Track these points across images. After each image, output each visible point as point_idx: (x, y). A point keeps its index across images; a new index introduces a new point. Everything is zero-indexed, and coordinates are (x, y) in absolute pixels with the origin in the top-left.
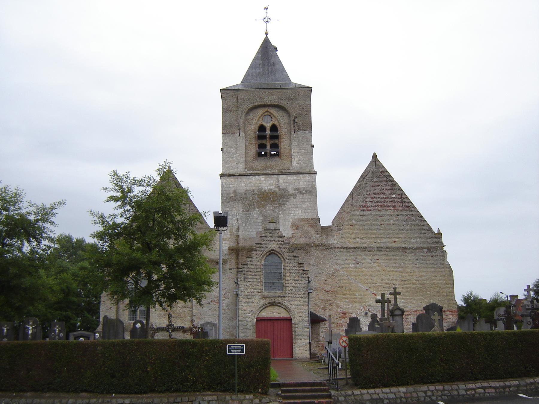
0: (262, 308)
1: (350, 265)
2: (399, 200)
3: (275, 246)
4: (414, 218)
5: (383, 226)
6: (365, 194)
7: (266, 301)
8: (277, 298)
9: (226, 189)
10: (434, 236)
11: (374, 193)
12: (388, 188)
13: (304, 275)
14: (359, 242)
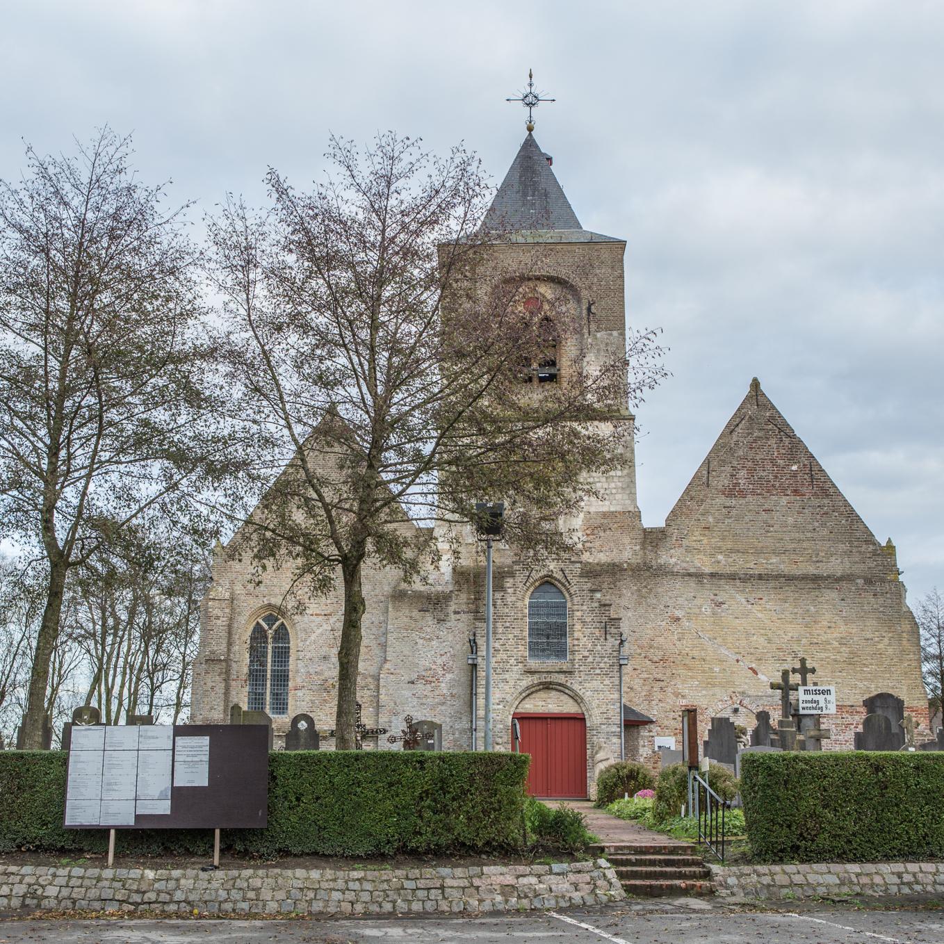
0: (524, 695)
2: (806, 476)
5: (772, 529)
6: (735, 463)
7: (535, 679)
11: (753, 460)
12: (784, 452)
14: (724, 563)
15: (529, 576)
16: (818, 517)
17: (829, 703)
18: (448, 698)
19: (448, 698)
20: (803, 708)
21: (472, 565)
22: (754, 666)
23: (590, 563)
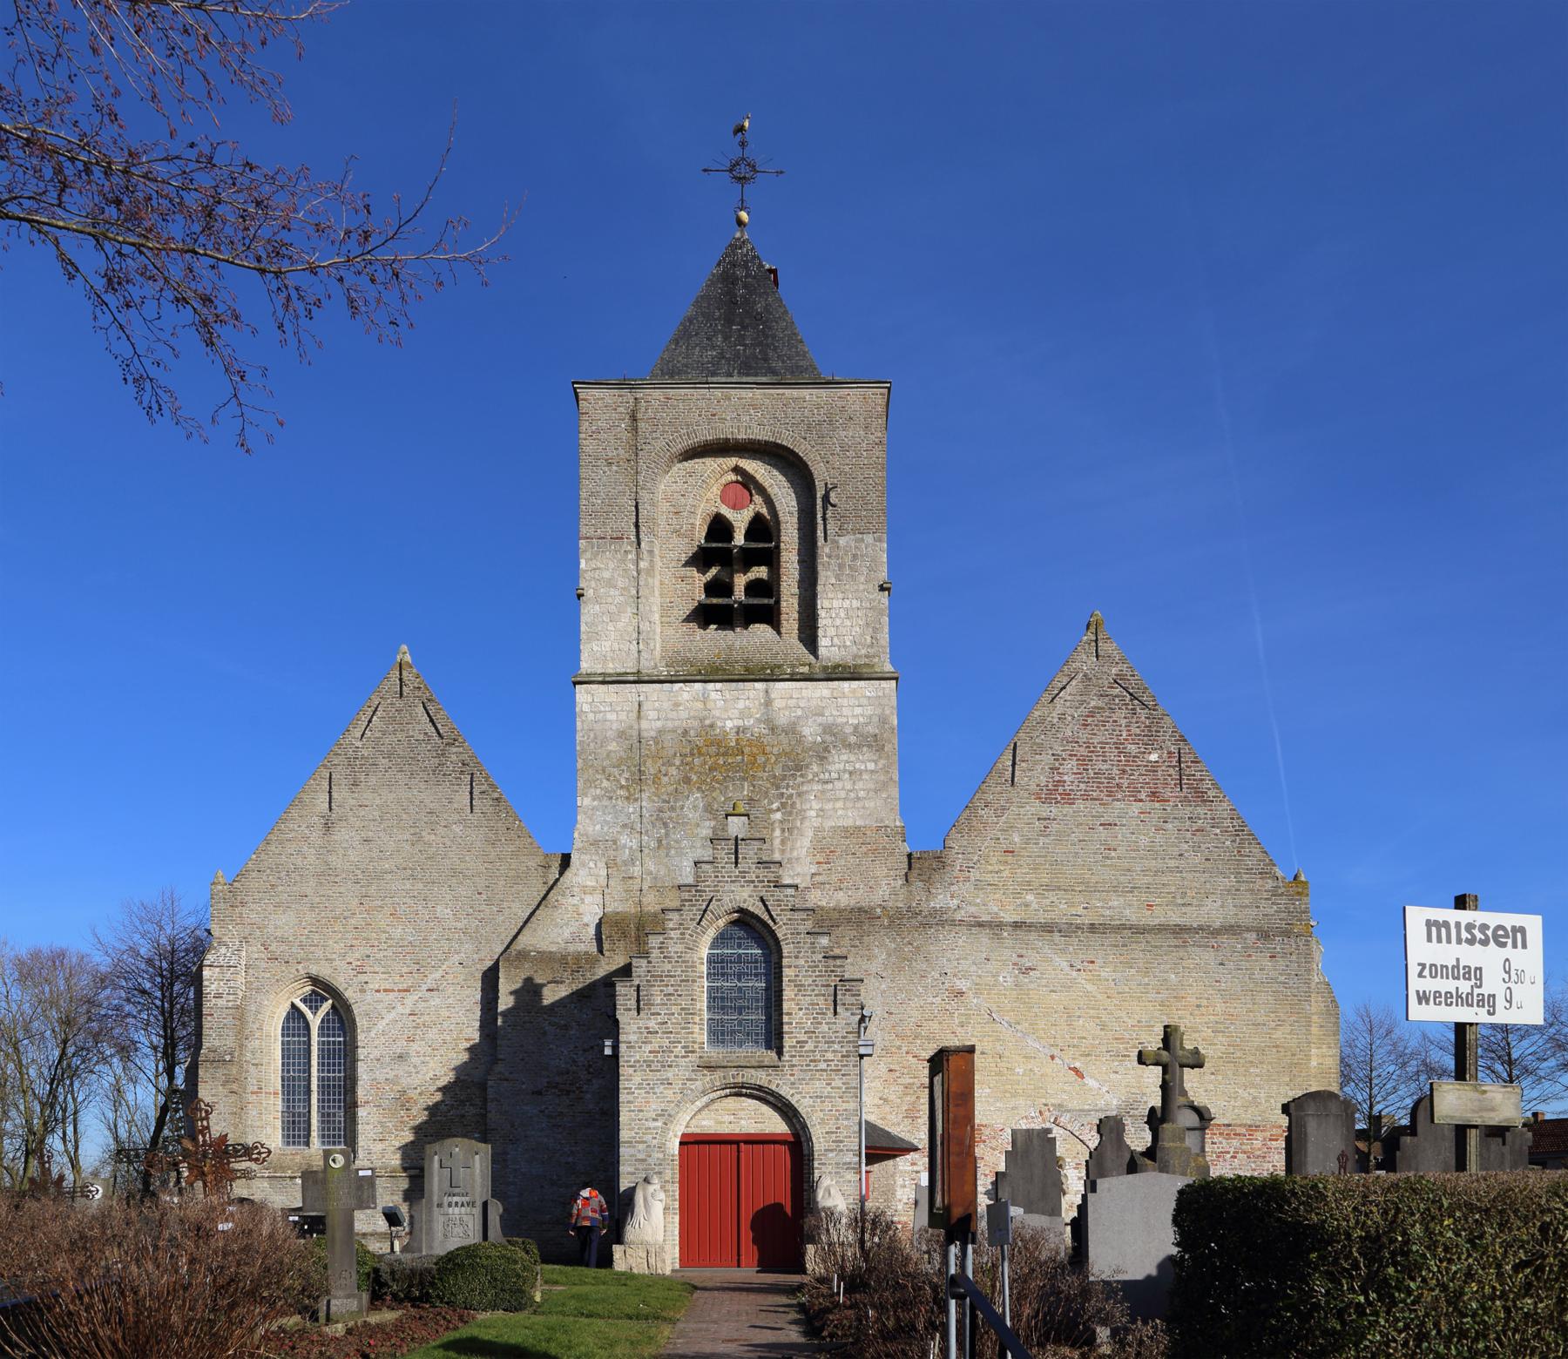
1: (1001, 979)
2: (1171, 771)
3: (745, 895)
4: (1218, 831)
6: (1058, 749)
8: (752, 1071)
10: (1280, 891)
11: (1088, 745)
14: (1035, 906)
15: (705, 911)
16: (1189, 835)
17: (1520, 981)
18: (597, 1116)
19: (597, 1116)
20: (1423, 998)
21: (633, 911)
22: (1077, 1065)
23: (822, 908)
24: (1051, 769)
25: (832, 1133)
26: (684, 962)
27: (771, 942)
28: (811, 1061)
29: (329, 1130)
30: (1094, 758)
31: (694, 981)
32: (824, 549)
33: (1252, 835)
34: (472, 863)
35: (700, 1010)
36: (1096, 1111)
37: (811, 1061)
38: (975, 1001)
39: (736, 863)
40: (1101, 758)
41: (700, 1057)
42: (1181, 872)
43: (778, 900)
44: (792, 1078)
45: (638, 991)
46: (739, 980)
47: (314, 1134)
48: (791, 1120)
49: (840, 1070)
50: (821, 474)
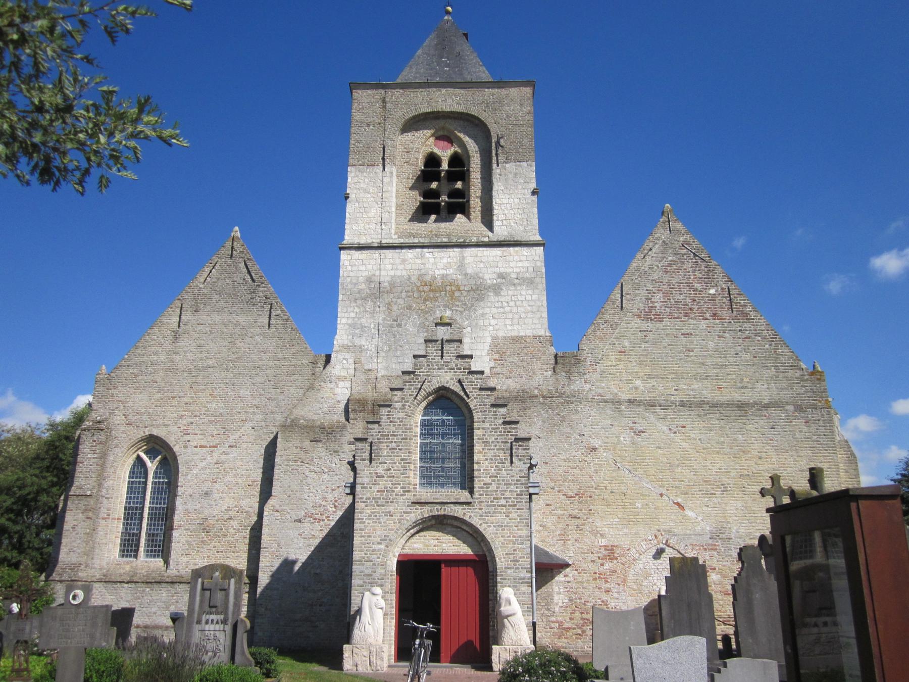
0: (412, 531)
1: (622, 439)
2: (724, 300)
3: (448, 378)
4: (759, 338)
5: (691, 353)
6: (650, 287)
7: (426, 512)
9: (351, 274)
10: (806, 378)
11: (669, 284)
12: (700, 275)
13: (520, 450)
14: (641, 387)
15: (420, 389)
16: (740, 341)
22: (679, 500)
24: (646, 299)
25: (510, 554)
26: (404, 425)
27: (465, 411)
28: (494, 498)
29: (152, 546)
30: (674, 292)
31: (410, 439)
32: (496, 170)
33: (782, 341)
34: (266, 361)
35: (414, 460)
36: (696, 535)
37: (494, 498)
38: (605, 454)
39: (442, 356)
40: (678, 292)
41: (414, 495)
42: (738, 365)
43: (470, 382)
44: (480, 511)
45: (371, 446)
46: (443, 438)
47: (142, 549)
48: (480, 544)
49: (515, 505)
50: (494, 130)
